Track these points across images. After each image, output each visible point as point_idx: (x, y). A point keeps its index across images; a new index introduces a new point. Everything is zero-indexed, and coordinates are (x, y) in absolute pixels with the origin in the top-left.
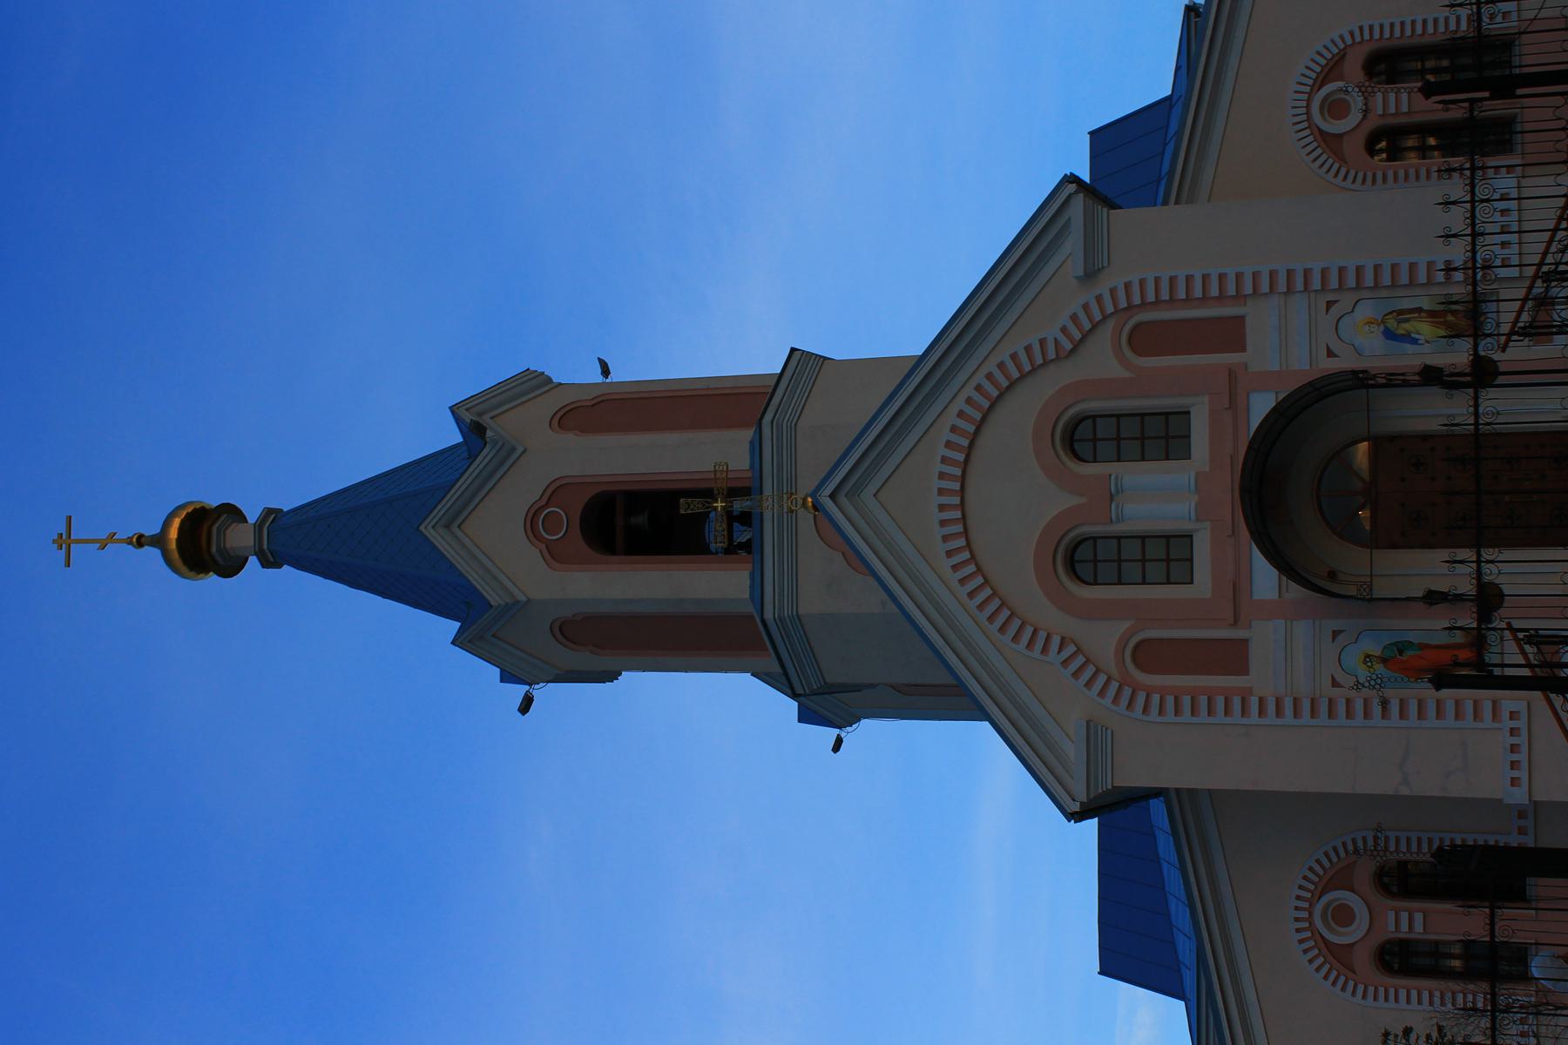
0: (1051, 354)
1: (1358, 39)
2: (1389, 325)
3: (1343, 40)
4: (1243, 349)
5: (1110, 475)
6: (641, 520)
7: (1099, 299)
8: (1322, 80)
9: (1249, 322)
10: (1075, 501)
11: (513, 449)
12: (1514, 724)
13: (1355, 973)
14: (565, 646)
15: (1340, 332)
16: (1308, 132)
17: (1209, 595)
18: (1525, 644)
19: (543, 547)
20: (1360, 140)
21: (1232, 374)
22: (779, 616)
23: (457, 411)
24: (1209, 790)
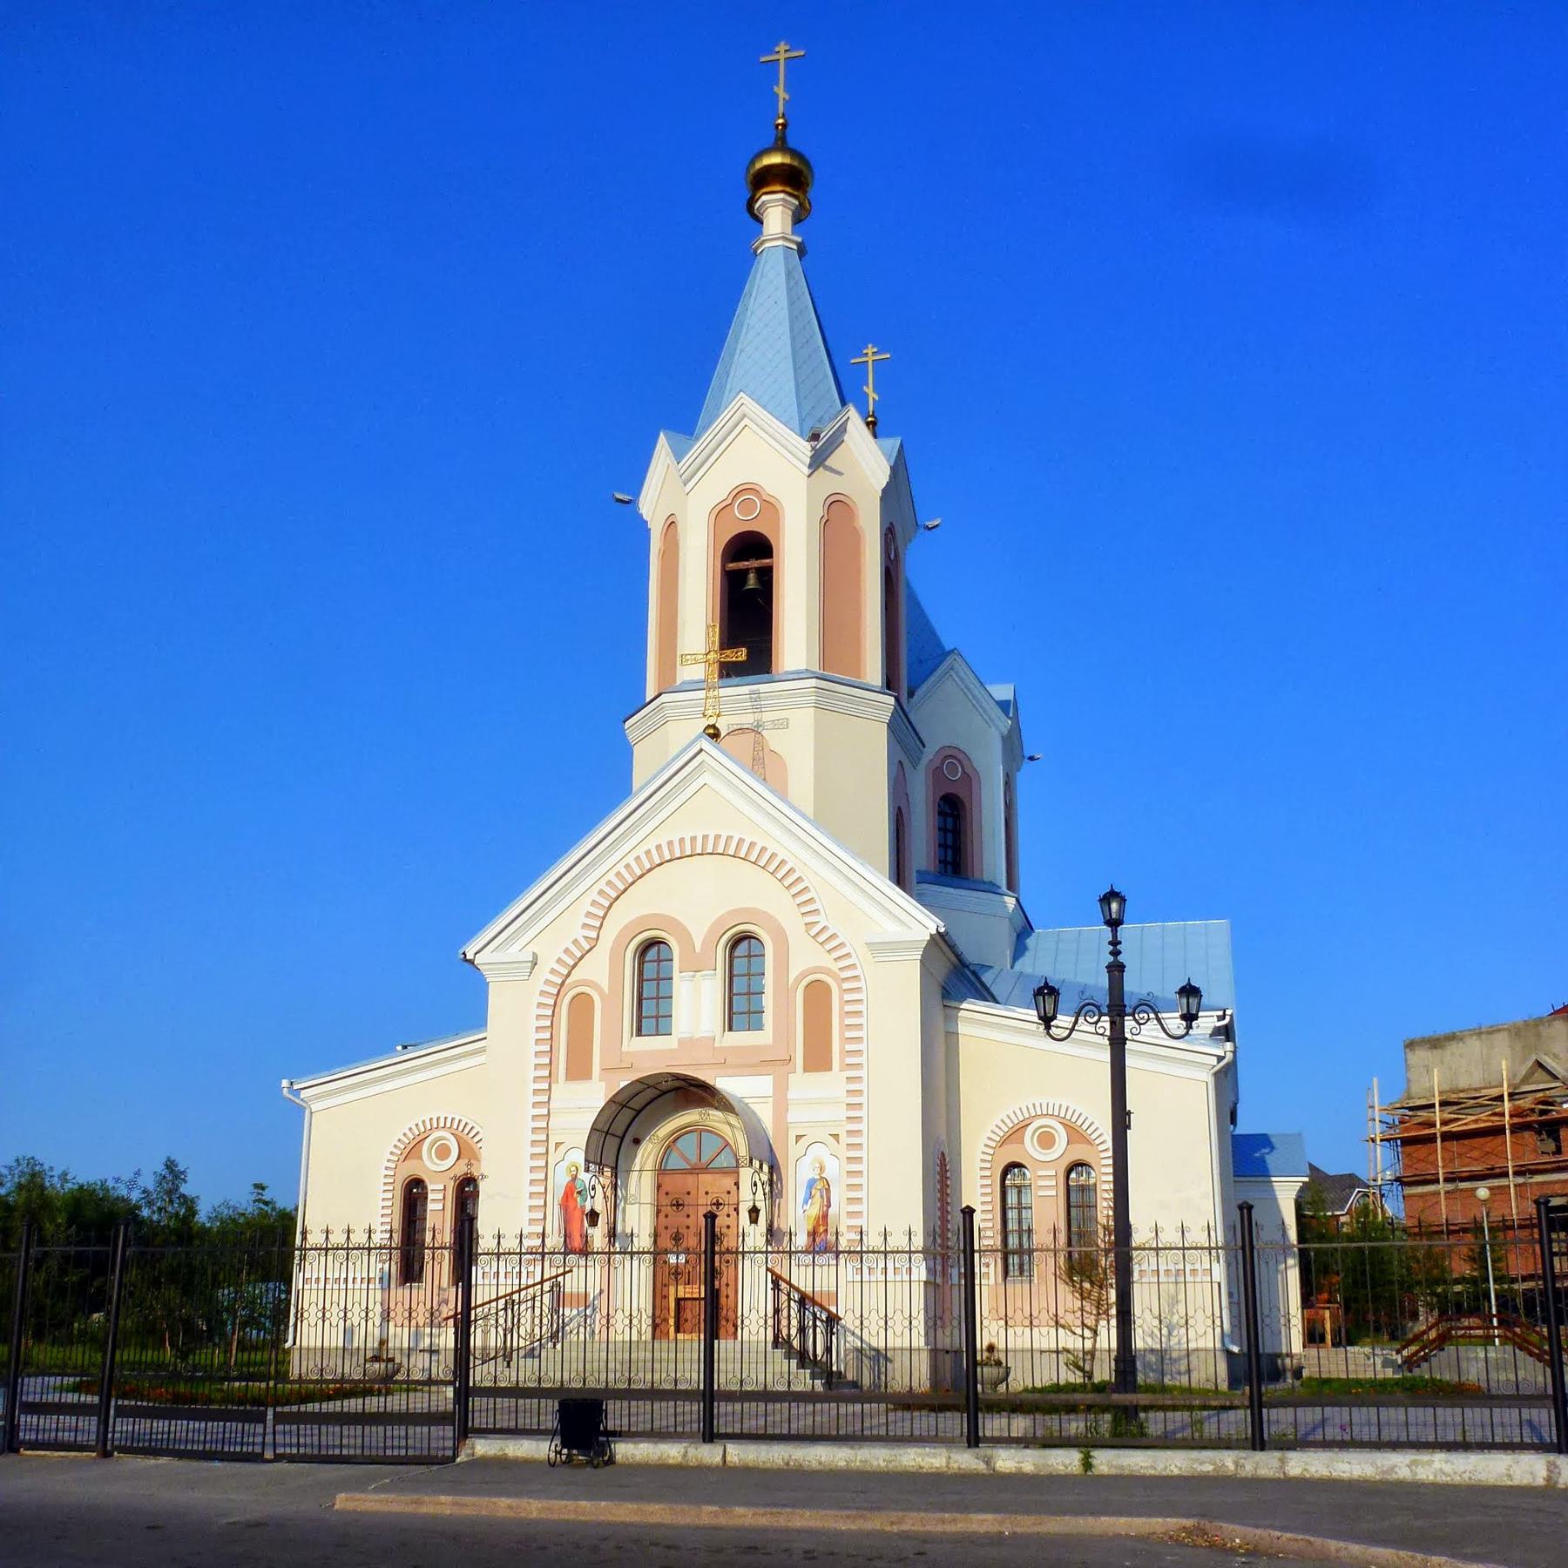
4: (806, 1070)
6: (752, 582)
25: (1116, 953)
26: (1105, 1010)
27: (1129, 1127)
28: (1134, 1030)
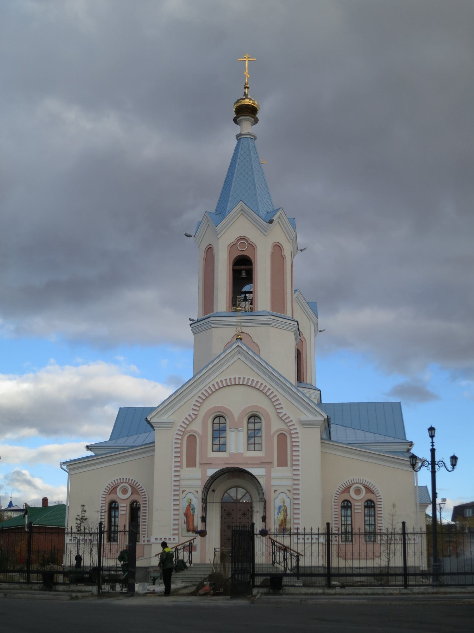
0: (278, 411)
1: (378, 498)
2: (282, 507)
3: (378, 493)
4: (278, 466)
5: (243, 428)
6: (244, 275)
7: (294, 425)
8: (366, 488)
9: (286, 468)
10: (236, 418)
11: (266, 232)
12: (172, 539)
13: (109, 495)
14: (205, 251)
15: (281, 493)
16: (351, 483)
17: (208, 456)
18: (190, 542)
19: (235, 243)
20: (348, 498)
21: (271, 463)
22: (211, 322)
23: (281, 210)
24: (154, 455)
25: (433, 446)
26: (430, 463)
27: (437, 497)
28: (438, 469)
